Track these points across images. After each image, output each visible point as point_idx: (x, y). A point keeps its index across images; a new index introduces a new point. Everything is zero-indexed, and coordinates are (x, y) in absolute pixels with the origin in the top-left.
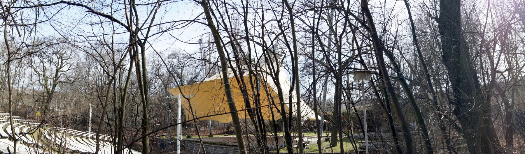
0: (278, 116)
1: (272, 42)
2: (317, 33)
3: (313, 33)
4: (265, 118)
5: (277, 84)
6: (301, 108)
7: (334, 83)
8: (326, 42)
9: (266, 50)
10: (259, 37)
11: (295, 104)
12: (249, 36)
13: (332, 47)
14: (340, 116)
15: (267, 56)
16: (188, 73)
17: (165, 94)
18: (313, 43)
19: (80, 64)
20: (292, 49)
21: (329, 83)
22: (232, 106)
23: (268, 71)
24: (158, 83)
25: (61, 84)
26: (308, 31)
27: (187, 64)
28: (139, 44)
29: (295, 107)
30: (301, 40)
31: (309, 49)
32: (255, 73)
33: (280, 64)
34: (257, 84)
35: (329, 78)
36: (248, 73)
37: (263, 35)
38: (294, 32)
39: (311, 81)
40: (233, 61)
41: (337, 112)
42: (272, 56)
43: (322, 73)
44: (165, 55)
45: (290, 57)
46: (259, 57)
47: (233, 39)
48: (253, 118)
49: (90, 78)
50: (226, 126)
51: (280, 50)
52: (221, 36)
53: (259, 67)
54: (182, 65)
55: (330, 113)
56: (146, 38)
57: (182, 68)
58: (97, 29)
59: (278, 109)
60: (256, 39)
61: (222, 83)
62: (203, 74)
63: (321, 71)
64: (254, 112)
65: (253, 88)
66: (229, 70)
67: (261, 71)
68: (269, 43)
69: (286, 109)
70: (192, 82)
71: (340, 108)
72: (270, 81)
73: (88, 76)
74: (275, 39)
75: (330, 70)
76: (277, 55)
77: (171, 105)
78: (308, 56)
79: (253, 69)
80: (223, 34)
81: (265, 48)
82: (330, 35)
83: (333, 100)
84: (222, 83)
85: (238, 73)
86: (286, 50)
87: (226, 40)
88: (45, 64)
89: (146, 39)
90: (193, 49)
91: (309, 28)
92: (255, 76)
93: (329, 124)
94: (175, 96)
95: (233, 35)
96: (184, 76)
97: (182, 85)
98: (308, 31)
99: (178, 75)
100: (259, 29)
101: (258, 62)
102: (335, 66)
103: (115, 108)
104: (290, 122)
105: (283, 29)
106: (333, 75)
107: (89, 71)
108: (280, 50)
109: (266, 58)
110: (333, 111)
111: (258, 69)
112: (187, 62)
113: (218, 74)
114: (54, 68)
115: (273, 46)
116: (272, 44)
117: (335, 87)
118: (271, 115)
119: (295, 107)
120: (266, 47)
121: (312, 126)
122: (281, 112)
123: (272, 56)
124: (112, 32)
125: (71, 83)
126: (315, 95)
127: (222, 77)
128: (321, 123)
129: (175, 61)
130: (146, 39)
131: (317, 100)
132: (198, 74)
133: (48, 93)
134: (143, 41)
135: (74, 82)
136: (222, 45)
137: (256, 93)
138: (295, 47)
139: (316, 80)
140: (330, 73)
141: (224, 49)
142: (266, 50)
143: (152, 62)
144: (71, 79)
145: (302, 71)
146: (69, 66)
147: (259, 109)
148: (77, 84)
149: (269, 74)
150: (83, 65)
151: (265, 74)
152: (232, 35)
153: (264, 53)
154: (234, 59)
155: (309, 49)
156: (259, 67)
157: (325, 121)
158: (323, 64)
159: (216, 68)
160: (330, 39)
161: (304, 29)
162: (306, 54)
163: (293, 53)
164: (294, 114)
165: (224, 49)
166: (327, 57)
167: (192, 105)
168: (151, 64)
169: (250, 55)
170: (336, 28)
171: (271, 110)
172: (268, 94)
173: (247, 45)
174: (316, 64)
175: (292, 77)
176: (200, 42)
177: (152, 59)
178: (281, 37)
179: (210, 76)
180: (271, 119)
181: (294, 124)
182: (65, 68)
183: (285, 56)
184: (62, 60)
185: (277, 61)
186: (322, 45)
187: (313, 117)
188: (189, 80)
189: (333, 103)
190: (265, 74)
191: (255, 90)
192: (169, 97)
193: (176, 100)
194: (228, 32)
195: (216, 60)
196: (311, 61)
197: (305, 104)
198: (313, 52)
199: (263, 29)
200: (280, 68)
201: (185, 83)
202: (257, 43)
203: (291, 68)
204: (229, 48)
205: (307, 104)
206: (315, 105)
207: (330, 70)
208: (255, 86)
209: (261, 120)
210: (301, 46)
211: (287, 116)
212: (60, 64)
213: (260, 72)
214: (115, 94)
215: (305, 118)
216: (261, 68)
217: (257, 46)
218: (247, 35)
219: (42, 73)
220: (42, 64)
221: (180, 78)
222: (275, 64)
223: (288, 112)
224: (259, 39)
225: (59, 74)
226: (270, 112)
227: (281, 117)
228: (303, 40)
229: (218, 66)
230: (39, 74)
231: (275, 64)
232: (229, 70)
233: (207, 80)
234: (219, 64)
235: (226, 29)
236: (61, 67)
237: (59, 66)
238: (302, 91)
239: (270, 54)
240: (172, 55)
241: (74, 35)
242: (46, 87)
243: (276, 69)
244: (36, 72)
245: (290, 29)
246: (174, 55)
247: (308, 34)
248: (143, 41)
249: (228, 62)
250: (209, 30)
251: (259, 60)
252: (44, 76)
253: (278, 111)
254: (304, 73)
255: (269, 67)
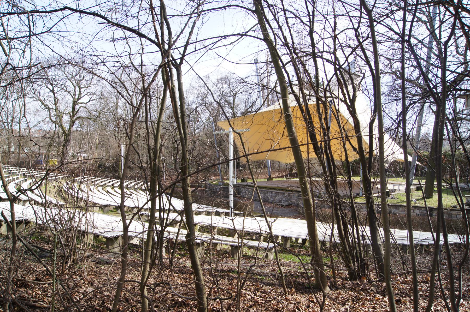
0: (353, 156)
1: (347, 58)
2: (409, 41)
3: (403, 41)
4: (336, 157)
5: (353, 113)
6: (385, 146)
7: (433, 111)
8: (422, 53)
9: (339, 69)
10: (329, 52)
11: (377, 139)
12: (316, 51)
13: (432, 60)
14: (440, 156)
15: (340, 77)
16: (241, 103)
17: (214, 128)
18: (403, 56)
19: (105, 93)
20: (373, 68)
21: (426, 111)
22: (293, 141)
23: (341, 96)
24: (204, 115)
25: (81, 120)
26: (396, 41)
27: (241, 91)
28: (173, 64)
29: (375, 145)
30: (386, 53)
31: (397, 66)
32: (324, 99)
33: (357, 88)
34: (326, 113)
35: (427, 105)
36: (314, 99)
37: (335, 50)
38: (374, 43)
39: (400, 109)
40: (295, 85)
41: (436, 151)
42: (347, 77)
43: (416, 98)
44: (214, 78)
45: (371, 78)
46: (329, 79)
47: (295, 56)
48: (320, 157)
49: (119, 111)
50: (289, 166)
51: (358, 69)
52: (280, 54)
53: (330, 91)
54: (234, 92)
55: (426, 152)
56: (184, 55)
57: (234, 97)
58: (121, 47)
59: (353, 147)
60: (326, 56)
61: (281, 113)
62: (259, 103)
63: (415, 95)
64: (324, 151)
65: (320, 119)
66: (291, 98)
67: (332, 97)
68: (342, 60)
69: (364, 146)
70: (246, 113)
71: (441, 146)
72: (344, 110)
73: (117, 108)
74: (351, 53)
75: (428, 92)
76: (353, 76)
77: (221, 143)
78: (396, 75)
79: (321, 94)
80: (282, 51)
81: (338, 67)
82: (430, 42)
83: (431, 135)
84: (281, 113)
85: (301, 101)
86: (366, 69)
87: (286, 59)
88: (56, 95)
89: (182, 59)
90: (247, 72)
91: (396, 37)
92: (324, 104)
93: (423, 168)
94: (226, 131)
95: (294, 52)
96: (237, 105)
97: (234, 115)
98: (396, 41)
99: (229, 104)
100: (330, 42)
101: (328, 85)
102: (435, 87)
103: (149, 148)
104: (369, 164)
105: (361, 40)
106: (433, 100)
107: (117, 103)
108: (358, 69)
109: (338, 80)
110: (430, 150)
111: (328, 94)
112: (240, 87)
113: (277, 103)
114: (70, 100)
115: (349, 63)
116: (347, 60)
117: (434, 116)
118: (344, 153)
119: (375, 145)
120: (339, 65)
121: (402, 170)
122: (358, 149)
123: (347, 77)
124: (141, 52)
125: (95, 119)
126: (404, 129)
127: (282, 107)
128: (412, 166)
129: (225, 86)
130: (182, 59)
131: (408, 134)
132: (254, 102)
133: (64, 132)
134: (178, 61)
135: (98, 116)
136: (281, 65)
137: (324, 125)
138: (376, 63)
139: (407, 108)
140: (428, 97)
141: (283, 70)
142: (339, 69)
143: (197, 89)
144: (94, 113)
145: (387, 95)
146: (90, 96)
147: (328, 146)
148: (103, 120)
149: (342, 101)
150: (109, 94)
151: (336, 101)
152: (292, 50)
153: (336, 73)
154: (297, 83)
155: (397, 66)
156: (330, 91)
157: (417, 163)
158: (418, 86)
159: (275, 94)
160: (430, 49)
161: (391, 39)
162: (393, 73)
163: (374, 72)
164: (375, 152)
165: (283, 70)
166: (424, 75)
167: (243, 141)
168: (195, 91)
169: (317, 77)
170: (440, 33)
171: (344, 147)
172: (340, 127)
173: (313, 64)
174: (407, 85)
175: (373, 104)
176: (256, 62)
177: (197, 85)
178: (359, 51)
179: (269, 105)
180: (344, 158)
181: (376, 166)
182: (84, 99)
183: (364, 77)
184: (80, 88)
185: (353, 83)
186: (417, 58)
187: (400, 156)
188: (243, 111)
189: (431, 138)
190: (336, 101)
191: (323, 121)
192: (219, 133)
193: (227, 135)
194: (288, 48)
195: (274, 84)
196: (399, 82)
197: (391, 140)
198: (403, 68)
199: (335, 42)
200: (357, 93)
201: (239, 114)
202: (328, 61)
203: (372, 91)
204: (290, 69)
205: (394, 139)
206: (404, 141)
207: (428, 92)
208: (323, 117)
209: (330, 159)
210: (387, 62)
211: (367, 156)
212: (77, 93)
213: (331, 99)
214: (147, 129)
215: (390, 159)
216: (331, 93)
217: (327, 64)
218: (314, 51)
219: (54, 107)
220: (51, 94)
221: (232, 108)
222: (350, 88)
223: (368, 150)
224: (329, 55)
225: (77, 107)
226: (343, 150)
227: (358, 157)
228: (389, 54)
229: (277, 92)
230: (49, 108)
231: (350, 88)
232: (291, 98)
233: (264, 110)
234: (278, 89)
235: (286, 44)
236: (79, 99)
237: (77, 97)
238: (387, 122)
239: (344, 75)
240: (222, 79)
241: (85, 52)
242: (61, 126)
243: (351, 94)
244: (45, 105)
245: (370, 40)
246: (224, 80)
247: (397, 44)
248: (178, 61)
249: (289, 88)
250: (264, 45)
251: (329, 82)
252: (56, 110)
253: (354, 149)
254: (390, 98)
255: (343, 92)
